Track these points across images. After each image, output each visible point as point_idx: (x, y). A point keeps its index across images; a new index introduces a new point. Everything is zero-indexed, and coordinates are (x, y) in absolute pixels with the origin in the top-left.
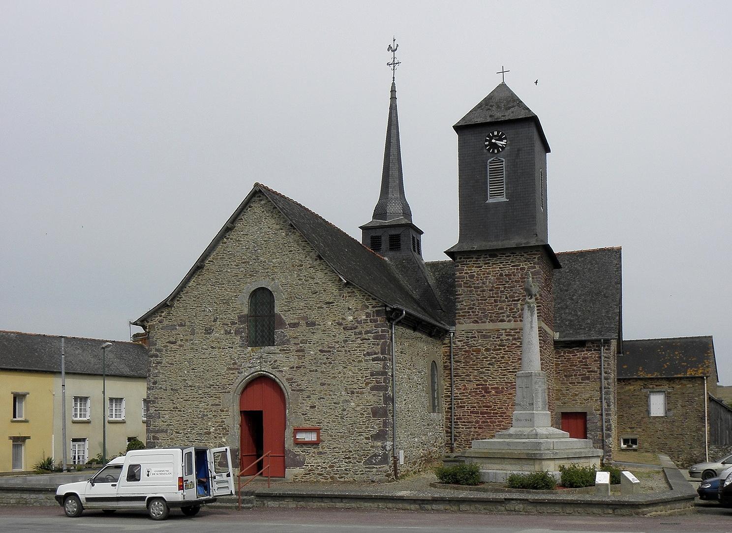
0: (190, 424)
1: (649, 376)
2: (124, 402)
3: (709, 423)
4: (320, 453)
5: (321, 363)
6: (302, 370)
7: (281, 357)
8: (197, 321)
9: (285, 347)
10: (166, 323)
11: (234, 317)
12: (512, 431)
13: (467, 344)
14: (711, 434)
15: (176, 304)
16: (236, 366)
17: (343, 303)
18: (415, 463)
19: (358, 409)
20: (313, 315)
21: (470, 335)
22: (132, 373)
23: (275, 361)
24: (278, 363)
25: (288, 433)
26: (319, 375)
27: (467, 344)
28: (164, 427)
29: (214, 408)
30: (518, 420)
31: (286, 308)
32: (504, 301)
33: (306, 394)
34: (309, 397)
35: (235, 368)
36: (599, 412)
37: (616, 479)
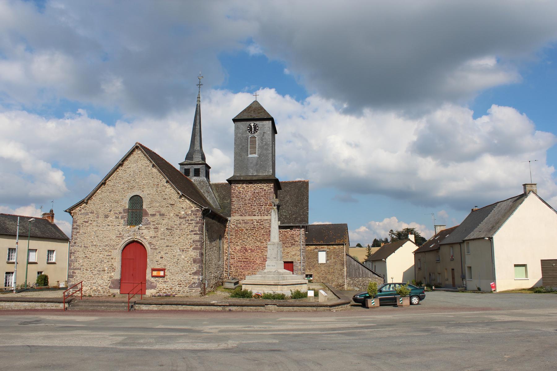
0: (94, 265)
1: (318, 243)
2: (55, 252)
3: (347, 267)
4: (165, 282)
7: (145, 231)
8: (100, 211)
10: (83, 211)
11: (121, 209)
12: (265, 271)
13: (237, 226)
14: (347, 272)
17: (179, 205)
18: (212, 287)
19: (186, 259)
20: (163, 211)
21: (238, 222)
24: (144, 235)
25: (148, 271)
26: (165, 241)
27: (237, 226)
28: (79, 267)
29: (108, 257)
31: (149, 206)
33: (158, 251)
34: (160, 252)
35: (120, 236)
37: (316, 294)
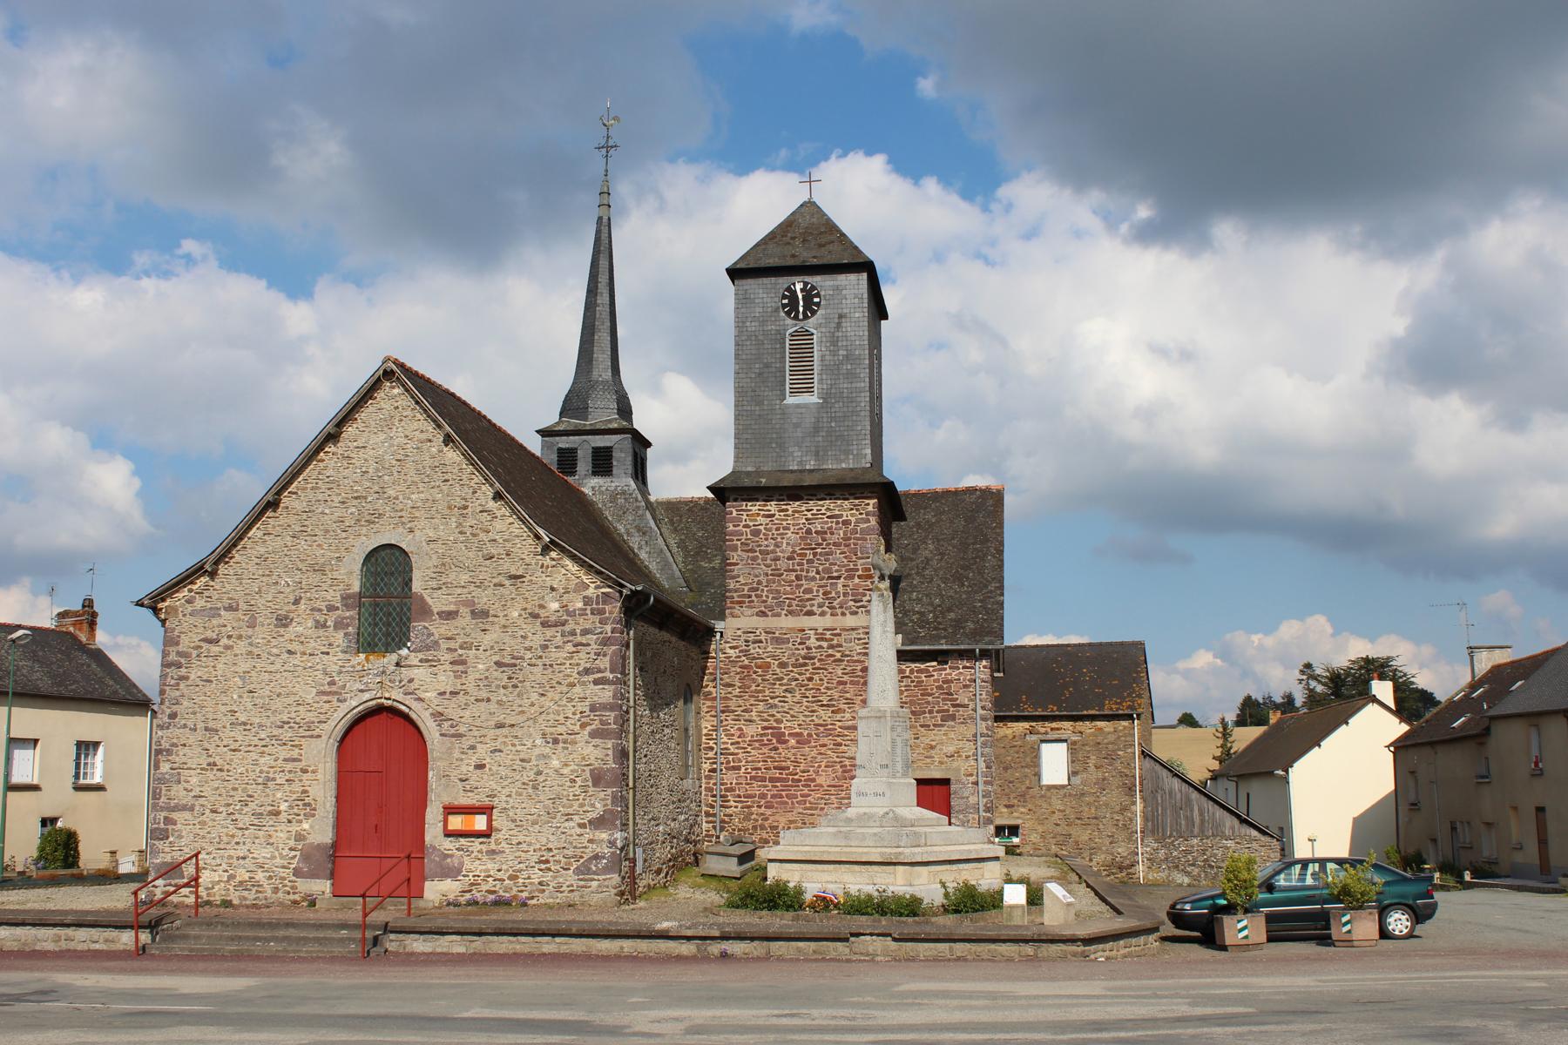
0: (239, 795)
4: (493, 852)
5: (498, 687)
6: (461, 698)
7: (420, 673)
9: (429, 655)
10: (200, 603)
11: (334, 596)
12: (851, 812)
13: (746, 653)
14: (1145, 819)
15: (222, 569)
16: (334, 688)
18: (659, 872)
19: (566, 771)
20: (484, 599)
21: (752, 637)
22: (55, 690)
23: (411, 681)
25: (433, 814)
26: (493, 706)
27: (746, 653)
29: (289, 766)
30: (859, 794)
31: (434, 584)
32: (813, 579)
35: (332, 692)
36: (972, 779)
37: (1035, 898)
